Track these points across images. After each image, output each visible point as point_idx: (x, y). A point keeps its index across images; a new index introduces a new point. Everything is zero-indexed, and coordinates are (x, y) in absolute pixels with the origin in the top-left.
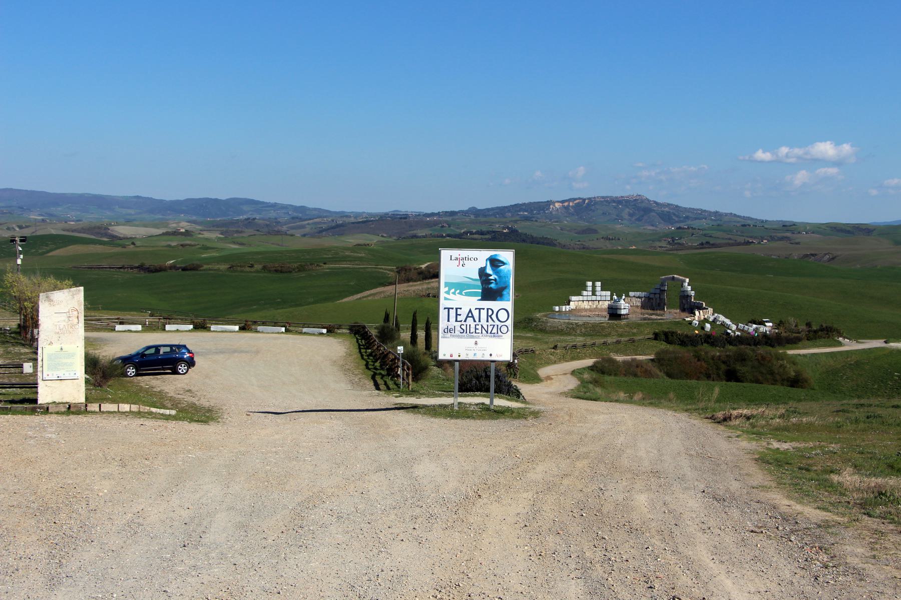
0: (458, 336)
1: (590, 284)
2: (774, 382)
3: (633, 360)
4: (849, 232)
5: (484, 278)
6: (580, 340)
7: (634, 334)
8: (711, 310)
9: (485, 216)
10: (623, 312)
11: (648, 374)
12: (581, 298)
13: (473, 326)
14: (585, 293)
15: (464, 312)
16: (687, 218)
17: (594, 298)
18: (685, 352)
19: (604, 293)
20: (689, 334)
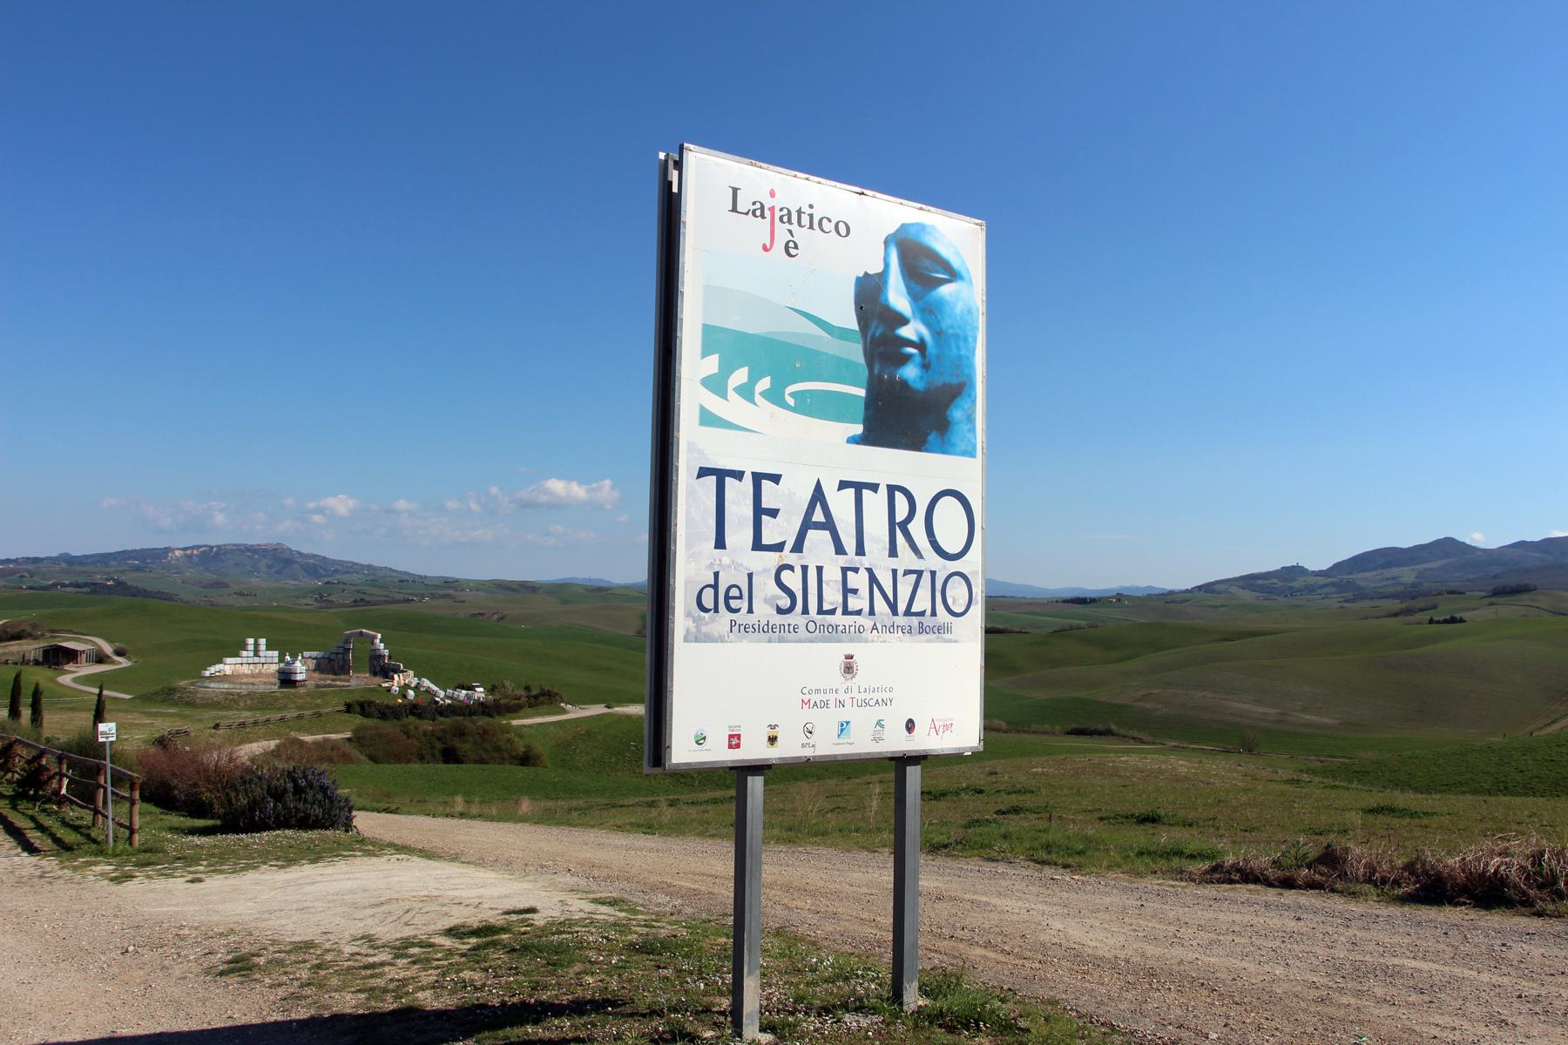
0: (767, 629)
1: (251, 641)
2: (502, 761)
3: (326, 740)
4: (514, 590)
5: (877, 330)
6: (246, 715)
7: (318, 706)
8: (411, 673)
9: (82, 564)
10: (299, 677)
11: (347, 758)
12: (239, 660)
13: (832, 575)
14: (244, 653)
15: (790, 498)
16: (336, 571)
17: (256, 660)
18: (388, 727)
19: (270, 653)
20: (391, 703)
